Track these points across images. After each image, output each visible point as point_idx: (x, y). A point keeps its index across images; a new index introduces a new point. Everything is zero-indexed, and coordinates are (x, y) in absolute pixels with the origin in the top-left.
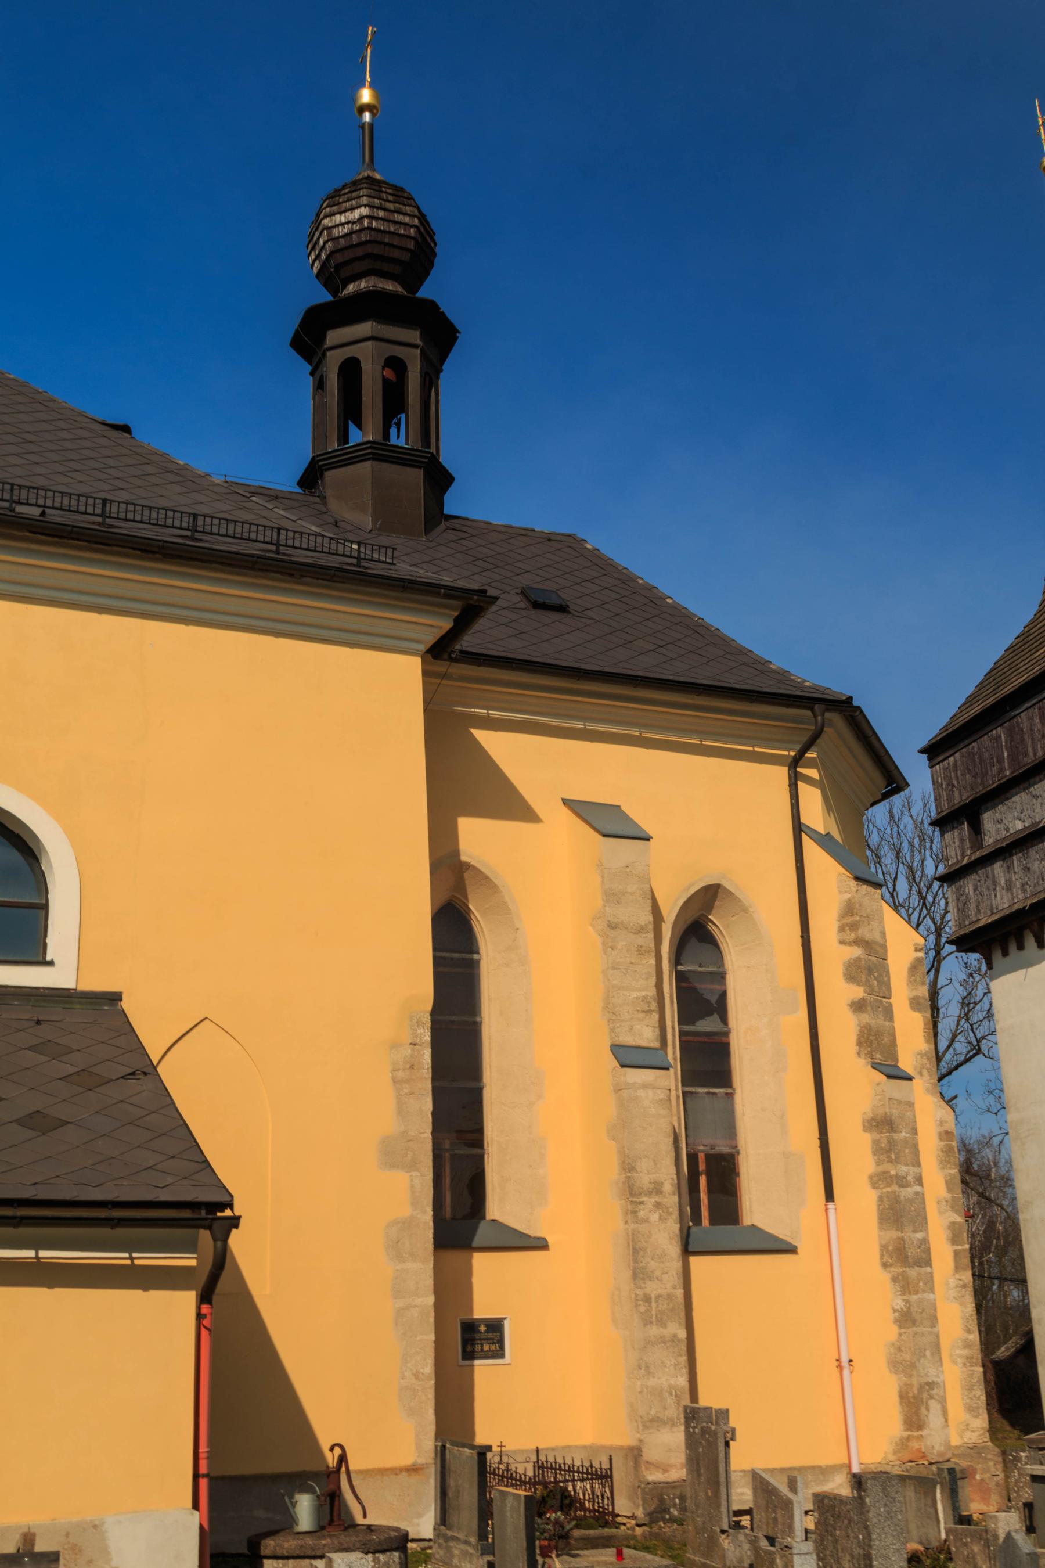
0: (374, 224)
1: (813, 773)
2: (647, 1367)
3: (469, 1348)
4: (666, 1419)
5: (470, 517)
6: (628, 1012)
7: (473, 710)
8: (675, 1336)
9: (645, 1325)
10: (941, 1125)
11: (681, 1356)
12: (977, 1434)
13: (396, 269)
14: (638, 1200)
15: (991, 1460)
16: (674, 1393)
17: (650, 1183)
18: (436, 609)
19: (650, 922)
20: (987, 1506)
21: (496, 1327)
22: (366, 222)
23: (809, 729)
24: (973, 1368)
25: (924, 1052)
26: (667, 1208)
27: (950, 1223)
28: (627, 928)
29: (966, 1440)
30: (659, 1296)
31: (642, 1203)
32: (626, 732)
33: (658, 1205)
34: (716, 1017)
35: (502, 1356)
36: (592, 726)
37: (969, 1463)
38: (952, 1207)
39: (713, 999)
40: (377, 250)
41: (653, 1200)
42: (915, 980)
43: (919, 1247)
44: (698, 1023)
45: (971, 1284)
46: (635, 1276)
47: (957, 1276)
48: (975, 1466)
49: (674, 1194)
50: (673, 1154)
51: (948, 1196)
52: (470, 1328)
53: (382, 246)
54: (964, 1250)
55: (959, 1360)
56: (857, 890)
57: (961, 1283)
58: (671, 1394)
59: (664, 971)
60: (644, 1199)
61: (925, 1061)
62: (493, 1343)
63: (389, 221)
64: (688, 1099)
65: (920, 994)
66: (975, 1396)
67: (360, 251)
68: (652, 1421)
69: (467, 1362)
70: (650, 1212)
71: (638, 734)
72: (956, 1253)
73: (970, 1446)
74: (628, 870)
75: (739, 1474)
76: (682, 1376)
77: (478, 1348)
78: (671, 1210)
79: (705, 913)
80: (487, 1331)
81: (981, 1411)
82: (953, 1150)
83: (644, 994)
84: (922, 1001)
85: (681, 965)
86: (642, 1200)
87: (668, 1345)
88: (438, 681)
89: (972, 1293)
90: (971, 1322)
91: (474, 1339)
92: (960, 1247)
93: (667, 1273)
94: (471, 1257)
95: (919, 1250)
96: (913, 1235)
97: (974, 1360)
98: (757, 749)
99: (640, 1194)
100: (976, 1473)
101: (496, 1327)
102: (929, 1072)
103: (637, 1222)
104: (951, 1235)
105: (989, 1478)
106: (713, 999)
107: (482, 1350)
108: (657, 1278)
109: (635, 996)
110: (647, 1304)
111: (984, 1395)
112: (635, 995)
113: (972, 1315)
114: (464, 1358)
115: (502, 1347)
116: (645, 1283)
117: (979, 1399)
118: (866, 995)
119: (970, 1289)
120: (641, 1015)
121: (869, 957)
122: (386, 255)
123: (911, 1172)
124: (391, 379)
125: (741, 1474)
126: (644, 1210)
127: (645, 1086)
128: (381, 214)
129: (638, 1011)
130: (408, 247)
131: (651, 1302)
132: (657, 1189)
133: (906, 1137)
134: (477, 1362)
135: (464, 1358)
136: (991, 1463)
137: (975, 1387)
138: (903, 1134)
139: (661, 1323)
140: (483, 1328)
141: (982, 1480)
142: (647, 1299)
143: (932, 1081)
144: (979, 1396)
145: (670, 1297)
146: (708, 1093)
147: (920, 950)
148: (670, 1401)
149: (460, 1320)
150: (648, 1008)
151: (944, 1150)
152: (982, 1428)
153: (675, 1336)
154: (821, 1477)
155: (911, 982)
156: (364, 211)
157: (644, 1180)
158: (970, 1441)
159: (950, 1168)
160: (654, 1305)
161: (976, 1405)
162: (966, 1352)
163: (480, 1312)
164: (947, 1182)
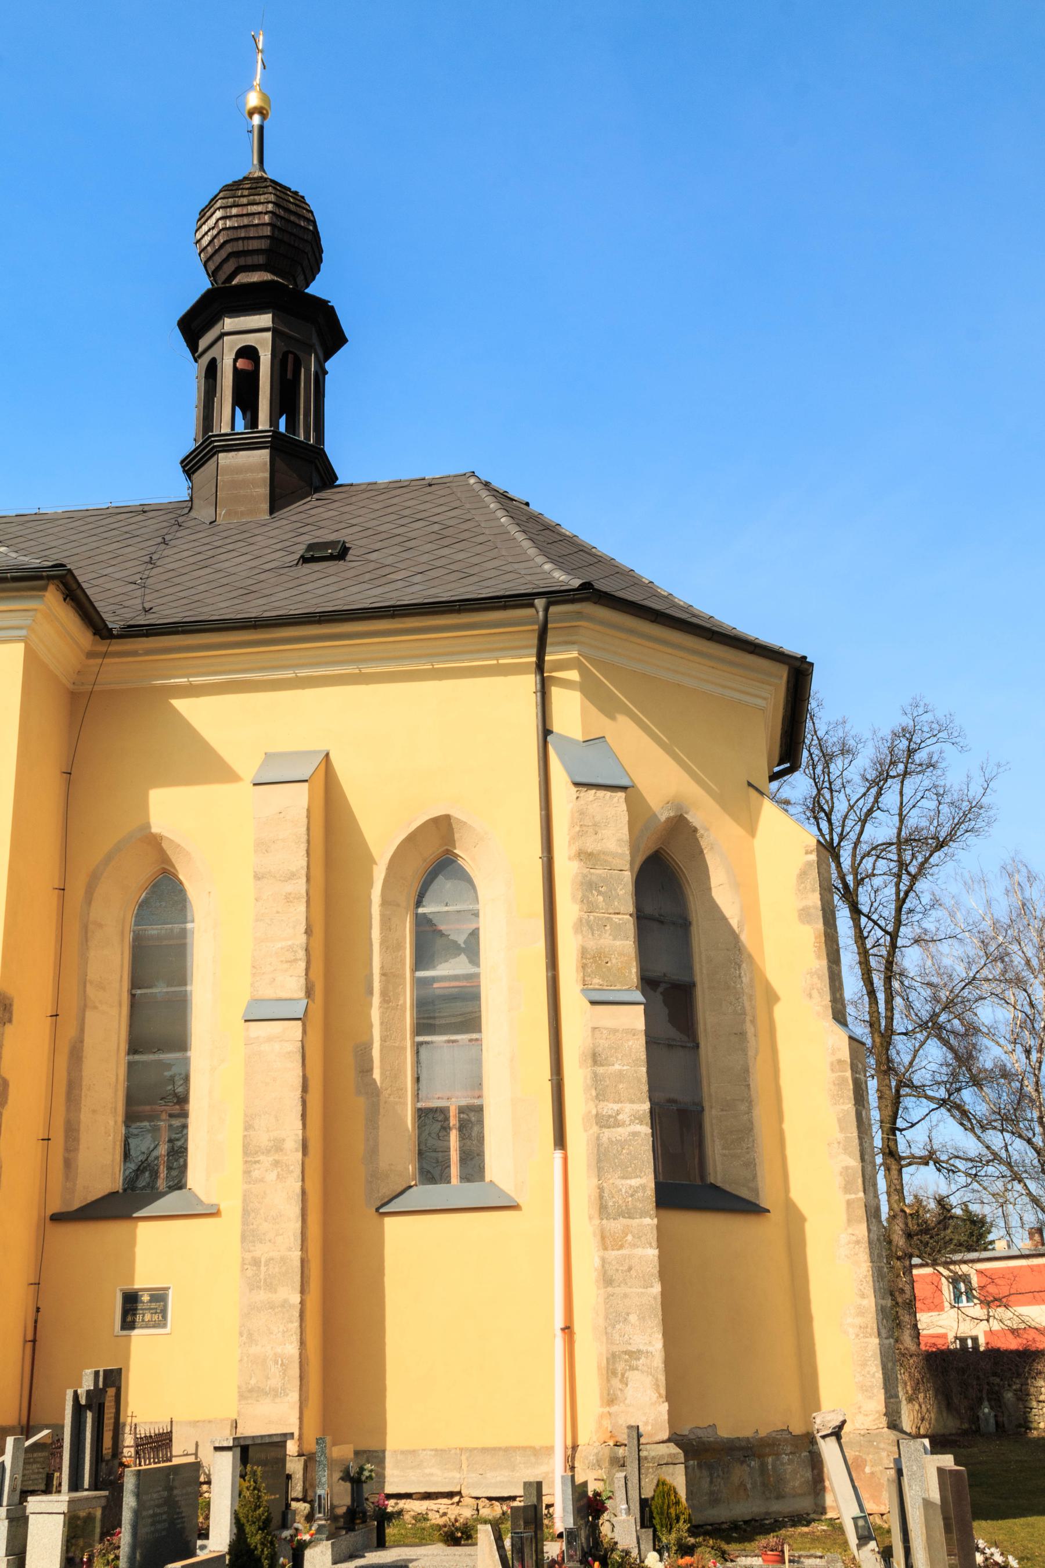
0: (229, 224)
1: (573, 675)
2: (250, 1335)
3: (129, 1319)
4: (268, 1388)
5: (354, 482)
6: (270, 964)
7: (172, 681)
8: (286, 1301)
9: (251, 1290)
10: (833, 1053)
11: (292, 1322)
12: (871, 1418)
13: (261, 259)
14: (253, 1160)
15: (883, 1449)
16: (280, 1362)
17: (269, 1140)
18: (25, 593)
19: (302, 867)
20: (877, 1505)
21: (160, 1297)
22: (221, 224)
23: (533, 630)
24: (867, 1340)
25: (814, 970)
26: (287, 1166)
27: (843, 1168)
28: (275, 877)
29: (858, 1426)
30: (269, 1260)
31: (258, 1162)
32: (343, 672)
33: (276, 1163)
34: (463, 958)
35: (164, 1326)
36: (303, 673)
37: (857, 1453)
38: (845, 1149)
39: (461, 940)
40: (240, 246)
41: (271, 1159)
42: (805, 888)
43: (632, 1196)
44: (440, 967)
45: (866, 1239)
46: (243, 1238)
47: (850, 1231)
48: (864, 1457)
49: (297, 1150)
50: (300, 1108)
51: (840, 1136)
52: (131, 1300)
53: (240, 242)
54: (859, 1199)
55: (851, 1330)
56: (577, 798)
57: (854, 1238)
58: (276, 1363)
59: (373, 916)
60: (261, 1158)
61: (816, 980)
62: (156, 1313)
63: (242, 215)
64: (423, 1050)
65: (810, 903)
66: (869, 1373)
67: (223, 254)
68: (251, 1391)
69: (125, 1333)
70: (266, 1171)
71: (357, 671)
72: (849, 1203)
73: (862, 1432)
74: (281, 815)
75: (429, 1453)
76: (292, 1343)
77: (139, 1318)
78: (292, 1168)
79: (449, 848)
80: (150, 1301)
81: (875, 1391)
82: (848, 1082)
83: (290, 943)
84: (812, 911)
85: (424, 906)
86: (257, 1159)
87: (276, 1310)
88: (99, 661)
89: (867, 1250)
90: (865, 1284)
91: (136, 1309)
92: (853, 1196)
93: (282, 1235)
94: (136, 1228)
95: (630, 1199)
96: (619, 1182)
97: (869, 1330)
98: (501, 661)
99: (256, 1153)
100: (865, 1466)
101: (160, 1297)
102: (819, 993)
103: (250, 1183)
104: (844, 1182)
105: (881, 1471)
106: (461, 940)
107: (143, 1321)
108: (270, 1241)
109: (280, 946)
110: (255, 1268)
111: (881, 1372)
112: (279, 945)
113: (866, 1276)
114: (123, 1328)
115: (165, 1317)
116: (254, 1246)
117: (873, 1376)
118: (583, 913)
119: (865, 1245)
120: (286, 966)
121: (592, 870)
122: (246, 249)
123: (627, 1110)
124: (246, 368)
125: (433, 1453)
126: (259, 1169)
127: (270, 1039)
128: (234, 211)
129: (282, 961)
130: (265, 234)
131: (260, 1266)
132: (277, 1146)
133: (620, 1071)
134: (136, 1332)
135: (123, 1328)
136: (884, 1454)
137: (869, 1363)
138: (617, 1067)
139: (270, 1287)
140: (146, 1298)
141: (872, 1473)
142: (256, 1262)
143: (824, 1003)
144: (874, 1374)
145: (283, 1260)
146: (449, 1041)
147: (811, 852)
148: (275, 1370)
149: (121, 1290)
150: (293, 958)
151: (837, 1082)
152: (877, 1412)
153: (286, 1301)
154: (533, 1459)
155: (799, 890)
156: (219, 214)
157: (262, 1138)
158: (862, 1427)
159: (843, 1103)
160: (263, 1268)
161: (870, 1384)
162: (859, 1321)
163: (140, 1282)
164: (839, 1120)
